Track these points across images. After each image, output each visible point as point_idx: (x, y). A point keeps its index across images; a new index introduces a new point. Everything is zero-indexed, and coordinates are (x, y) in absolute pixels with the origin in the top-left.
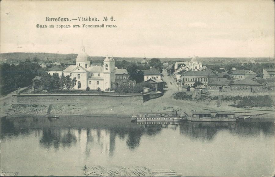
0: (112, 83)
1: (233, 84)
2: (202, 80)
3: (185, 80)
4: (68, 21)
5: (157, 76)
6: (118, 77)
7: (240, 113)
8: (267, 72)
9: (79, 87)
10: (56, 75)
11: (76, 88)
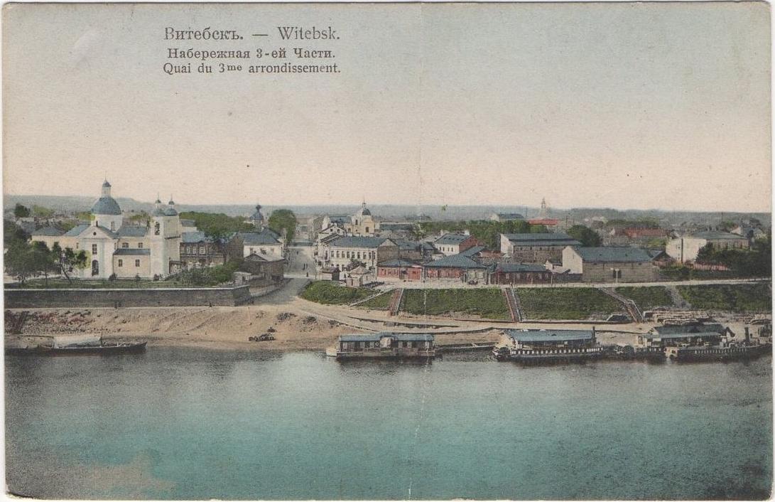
3: (329, 255)
6: (188, 249)
8: (508, 240)
9: (95, 272)
10: (42, 245)
11: (87, 273)
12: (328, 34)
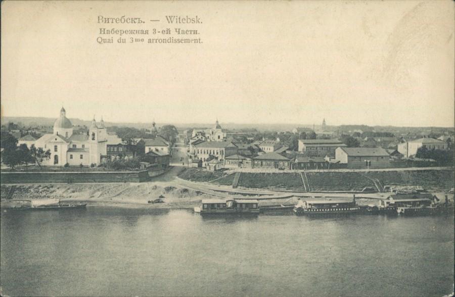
1: (257, 157)
5: (162, 147)
9: (56, 161)
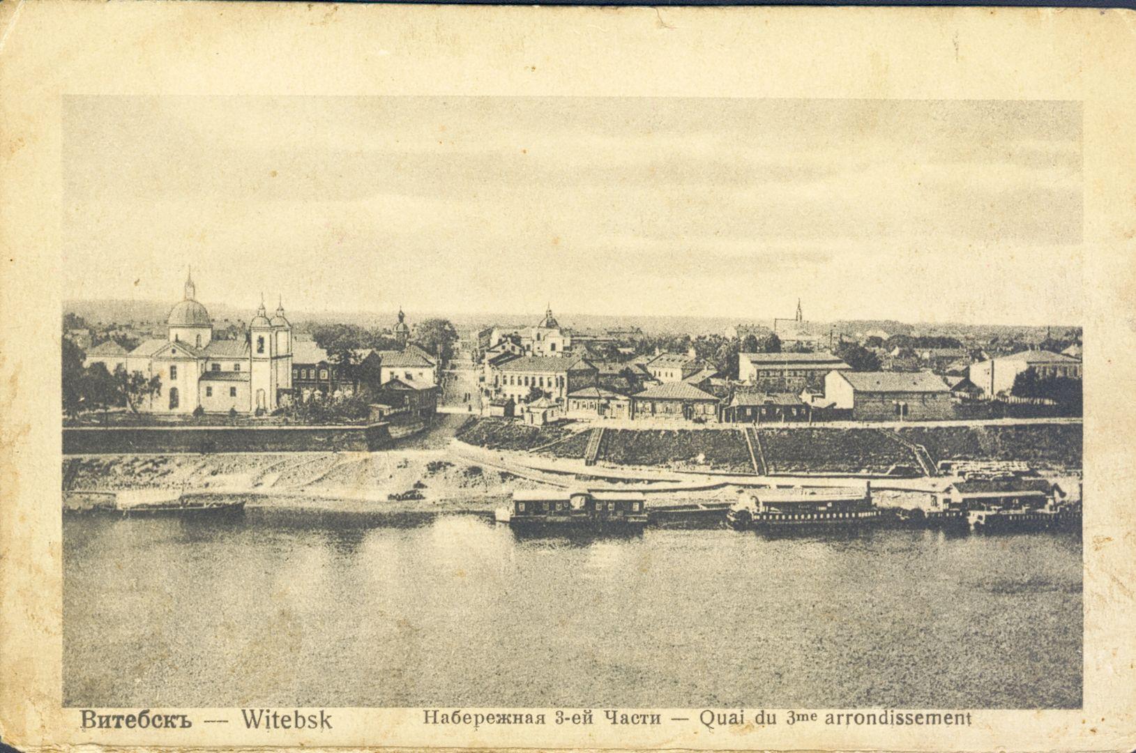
0: (646, 348)
2: (541, 384)
4: (183, 726)
7: (560, 473)
9: (174, 403)
12: (318, 720)
